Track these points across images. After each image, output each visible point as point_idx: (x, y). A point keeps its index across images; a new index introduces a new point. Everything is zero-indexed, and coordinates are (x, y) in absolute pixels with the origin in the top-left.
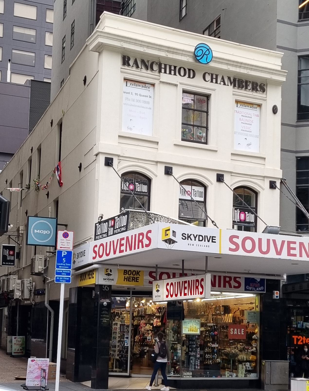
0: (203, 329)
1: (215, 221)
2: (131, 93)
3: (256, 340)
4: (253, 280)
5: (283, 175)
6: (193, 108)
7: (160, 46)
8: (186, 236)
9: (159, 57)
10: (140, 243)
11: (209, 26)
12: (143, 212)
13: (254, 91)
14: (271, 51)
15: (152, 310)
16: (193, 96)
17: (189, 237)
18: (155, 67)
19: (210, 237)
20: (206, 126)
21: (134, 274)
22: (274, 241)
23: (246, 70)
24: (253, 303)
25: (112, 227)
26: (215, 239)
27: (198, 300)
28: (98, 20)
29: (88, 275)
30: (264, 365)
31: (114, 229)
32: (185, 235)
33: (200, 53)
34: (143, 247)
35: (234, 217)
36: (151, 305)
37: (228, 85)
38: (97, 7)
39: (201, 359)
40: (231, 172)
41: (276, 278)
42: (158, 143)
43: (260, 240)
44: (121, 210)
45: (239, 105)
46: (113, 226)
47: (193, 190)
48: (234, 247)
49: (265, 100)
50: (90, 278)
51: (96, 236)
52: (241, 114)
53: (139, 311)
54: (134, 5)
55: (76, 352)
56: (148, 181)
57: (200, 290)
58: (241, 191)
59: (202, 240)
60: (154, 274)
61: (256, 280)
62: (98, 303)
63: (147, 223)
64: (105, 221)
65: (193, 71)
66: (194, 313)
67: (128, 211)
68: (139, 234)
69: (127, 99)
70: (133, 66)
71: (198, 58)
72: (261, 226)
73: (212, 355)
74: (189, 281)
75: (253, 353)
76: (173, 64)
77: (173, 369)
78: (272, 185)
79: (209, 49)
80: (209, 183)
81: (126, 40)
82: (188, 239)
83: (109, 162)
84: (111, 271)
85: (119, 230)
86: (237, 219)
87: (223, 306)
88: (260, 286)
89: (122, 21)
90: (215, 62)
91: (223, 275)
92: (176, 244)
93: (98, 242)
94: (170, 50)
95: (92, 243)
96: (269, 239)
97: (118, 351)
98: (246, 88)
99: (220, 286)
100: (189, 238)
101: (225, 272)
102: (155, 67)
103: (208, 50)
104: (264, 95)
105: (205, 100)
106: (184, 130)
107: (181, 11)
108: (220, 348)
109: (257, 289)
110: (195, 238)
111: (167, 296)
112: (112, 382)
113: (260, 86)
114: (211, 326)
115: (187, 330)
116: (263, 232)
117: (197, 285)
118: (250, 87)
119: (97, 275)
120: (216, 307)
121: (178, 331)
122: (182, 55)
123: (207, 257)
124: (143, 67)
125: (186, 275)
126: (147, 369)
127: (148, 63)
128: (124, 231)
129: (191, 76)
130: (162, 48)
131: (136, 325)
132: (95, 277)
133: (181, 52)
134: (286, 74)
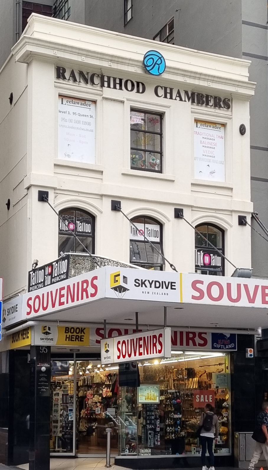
0: (163, 398)
1: (174, 265)
2: (67, 113)
3: (227, 408)
4: (222, 336)
5: (254, 209)
6: (143, 129)
7: (101, 54)
8: (140, 282)
9: (101, 68)
10: (84, 293)
11: (161, 31)
12: (86, 256)
13: (217, 108)
14: (236, 59)
15: (101, 378)
16: (143, 114)
17: (143, 283)
18: (97, 81)
19: (169, 282)
20: (159, 151)
21: (78, 332)
22: (246, 286)
23: (206, 82)
24: (222, 364)
25: (49, 274)
26: (175, 286)
27: (156, 363)
28: (25, 23)
29: (22, 335)
30: (237, 439)
31: (52, 278)
32: (139, 280)
33: (150, 63)
34: (87, 297)
35: (197, 260)
36: (99, 371)
37: (185, 101)
38: (23, 13)
39: (161, 433)
40: (192, 207)
41: (249, 333)
42: (102, 172)
43: (229, 285)
44: (59, 255)
45: (199, 125)
46: (51, 274)
47: (146, 229)
48: (197, 294)
49: (230, 118)
50: (24, 339)
51: (29, 286)
52: (202, 136)
53: (84, 379)
54: (69, 9)
55: (10, 431)
56: (91, 219)
57: (159, 347)
58: (204, 230)
59: (159, 287)
60: (102, 332)
61: (226, 336)
62: (34, 368)
63: (92, 268)
64: (40, 269)
65: (143, 84)
66: (151, 378)
67: (69, 255)
68: (83, 282)
69: (63, 119)
70: (69, 80)
71: (148, 69)
72: (229, 269)
73: (175, 428)
74: (144, 338)
75: (223, 424)
76: (118, 76)
77: (128, 447)
78: (242, 221)
79: (161, 58)
80: (165, 219)
81: (60, 47)
82: (142, 286)
83: (43, 197)
84: (49, 329)
85: (58, 279)
86: (201, 263)
87: (186, 369)
88: (231, 343)
89: (54, 25)
90: (169, 72)
91: (185, 330)
92: (127, 292)
93: (33, 294)
94: (114, 59)
95: (26, 296)
96: (240, 284)
97: (61, 427)
98: (207, 104)
99: (182, 344)
100: (143, 285)
101: (187, 327)
102: (97, 81)
103: (160, 58)
104: (228, 113)
105: (157, 120)
106: (134, 156)
107: (125, 14)
108: (183, 419)
109: (227, 347)
110: (151, 284)
111: (119, 357)
112: (54, 464)
113: (223, 101)
114: (173, 393)
115: (144, 398)
116: (232, 276)
117: (155, 342)
118: (212, 103)
119: (33, 334)
120: (178, 370)
121: (132, 401)
122: (128, 64)
123: (165, 308)
124: (81, 81)
125: (141, 331)
126: (96, 450)
127: (88, 76)
128: (64, 279)
129: (141, 91)
130: (105, 57)
131: (81, 397)
132: (30, 337)
133: (127, 62)
134: (254, 87)
